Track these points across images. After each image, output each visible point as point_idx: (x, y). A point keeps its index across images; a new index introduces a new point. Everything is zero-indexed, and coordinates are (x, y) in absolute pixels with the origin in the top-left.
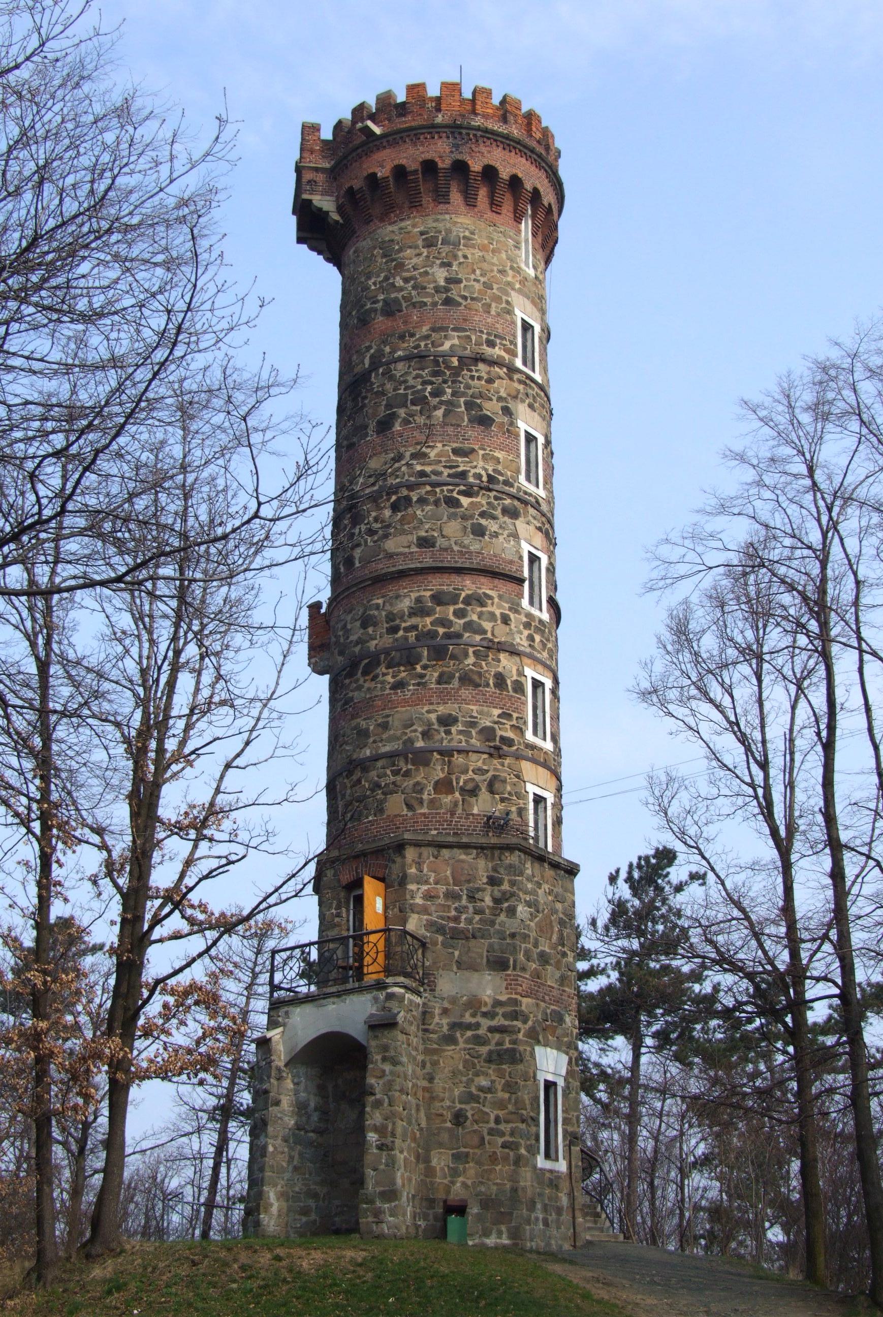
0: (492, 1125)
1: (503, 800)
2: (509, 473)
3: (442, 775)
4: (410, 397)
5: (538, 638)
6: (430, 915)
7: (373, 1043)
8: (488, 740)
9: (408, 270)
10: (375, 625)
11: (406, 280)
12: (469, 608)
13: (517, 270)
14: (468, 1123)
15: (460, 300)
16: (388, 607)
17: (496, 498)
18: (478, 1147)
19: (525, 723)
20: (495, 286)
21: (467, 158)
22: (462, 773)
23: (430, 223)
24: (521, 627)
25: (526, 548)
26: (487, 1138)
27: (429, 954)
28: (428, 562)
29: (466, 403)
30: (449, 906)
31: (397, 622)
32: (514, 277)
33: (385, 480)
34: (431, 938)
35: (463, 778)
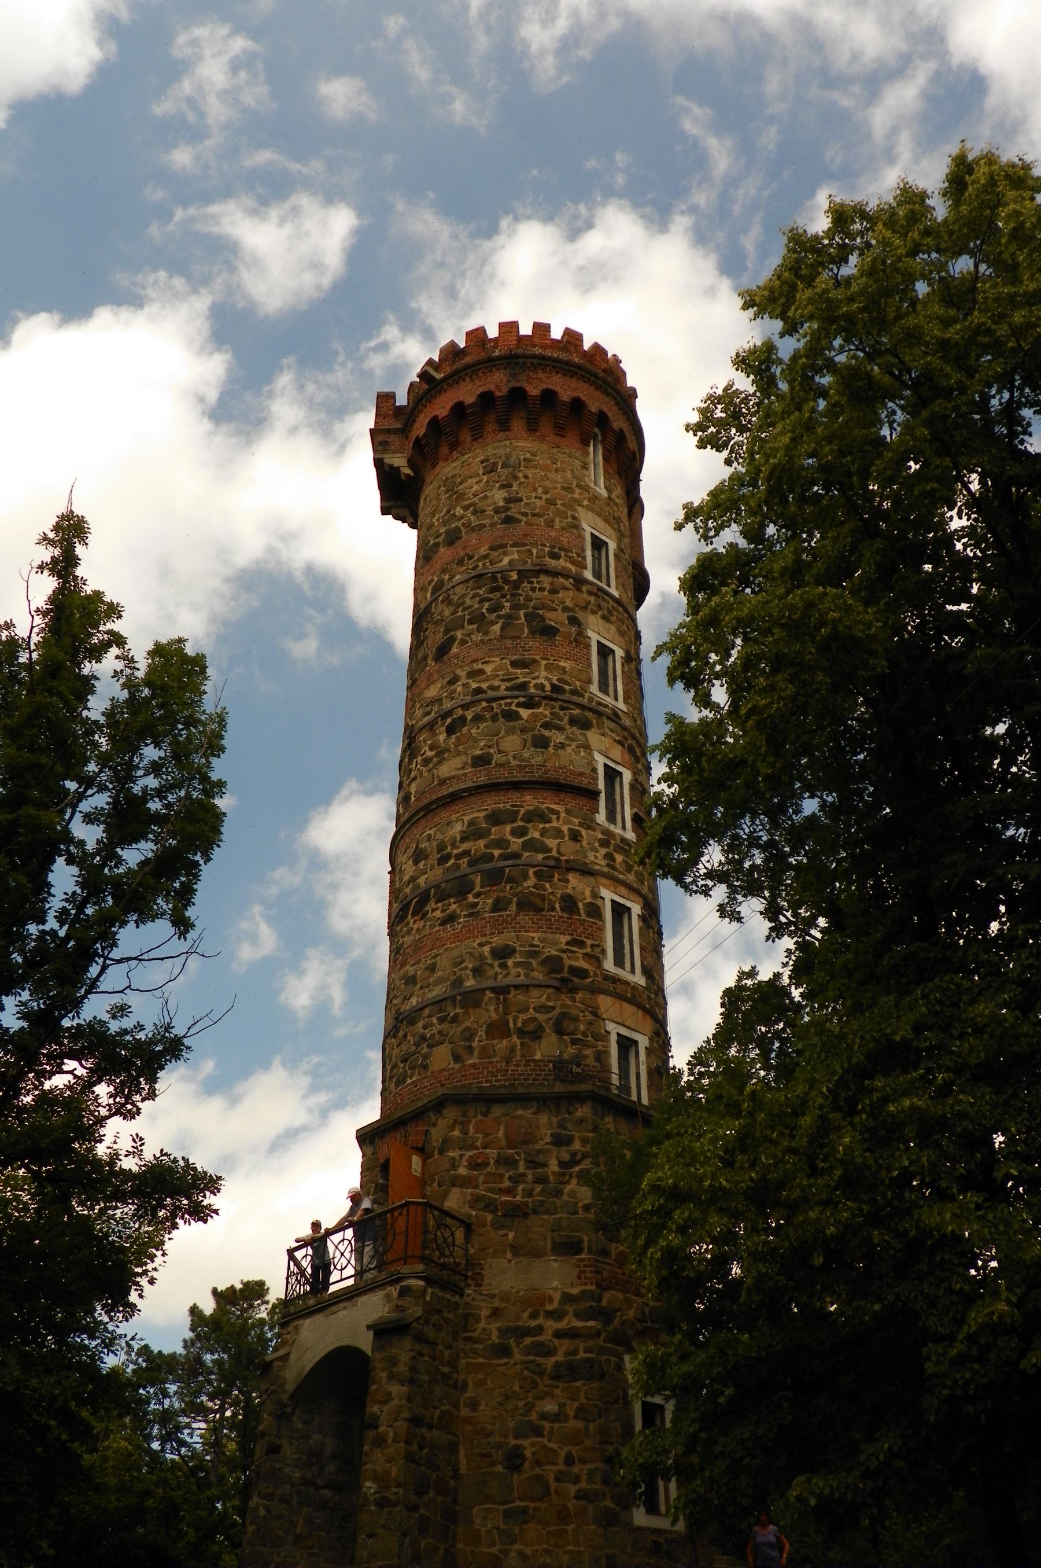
0: (561, 1467)
1: (574, 1042)
2: (578, 683)
3: (494, 1016)
4: (467, 617)
5: (619, 858)
6: (476, 1187)
7: (379, 1356)
8: (552, 971)
9: (468, 499)
10: (426, 857)
11: (466, 508)
12: (529, 825)
13: (586, 489)
14: (527, 1465)
15: (521, 517)
16: (440, 836)
17: (562, 708)
18: (540, 1499)
19: (604, 951)
20: (559, 502)
21: (524, 385)
22: (520, 1012)
23: (490, 451)
24: (597, 844)
25: (600, 760)
26: (553, 1485)
27: (476, 1239)
28: (482, 779)
29: (526, 615)
30: (502, 1176)
31: (449, 850)
32: (581, 494)
33: (441, 704)
34: (476, 1217)
35: (523, 1017)
